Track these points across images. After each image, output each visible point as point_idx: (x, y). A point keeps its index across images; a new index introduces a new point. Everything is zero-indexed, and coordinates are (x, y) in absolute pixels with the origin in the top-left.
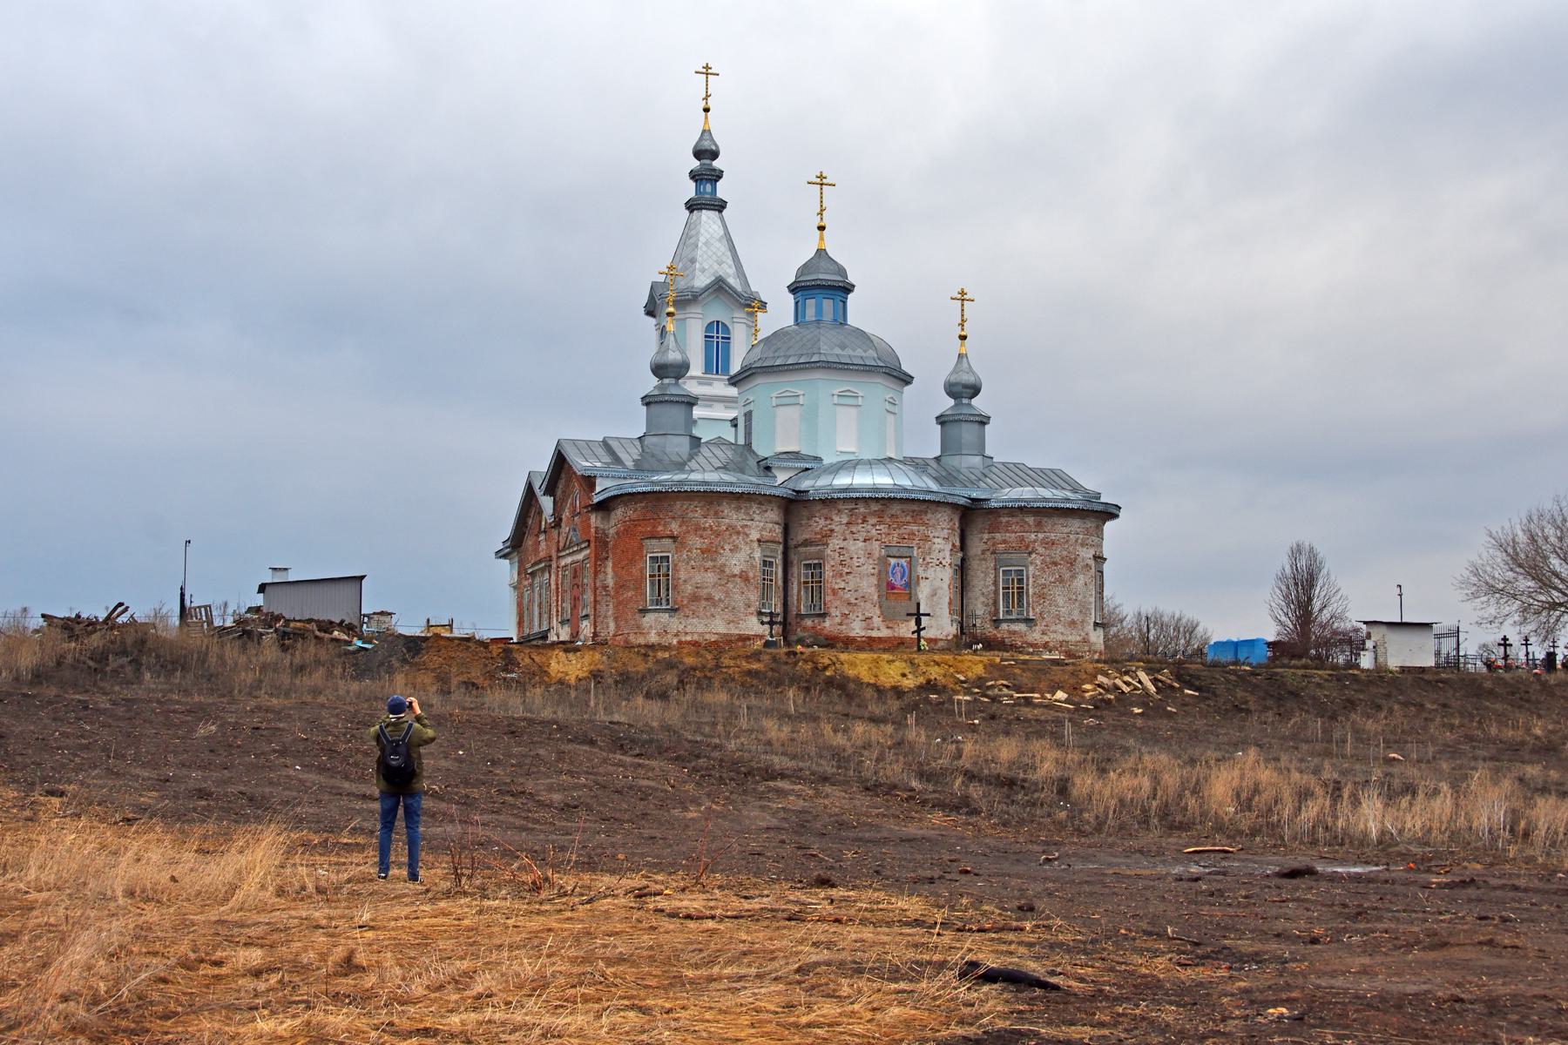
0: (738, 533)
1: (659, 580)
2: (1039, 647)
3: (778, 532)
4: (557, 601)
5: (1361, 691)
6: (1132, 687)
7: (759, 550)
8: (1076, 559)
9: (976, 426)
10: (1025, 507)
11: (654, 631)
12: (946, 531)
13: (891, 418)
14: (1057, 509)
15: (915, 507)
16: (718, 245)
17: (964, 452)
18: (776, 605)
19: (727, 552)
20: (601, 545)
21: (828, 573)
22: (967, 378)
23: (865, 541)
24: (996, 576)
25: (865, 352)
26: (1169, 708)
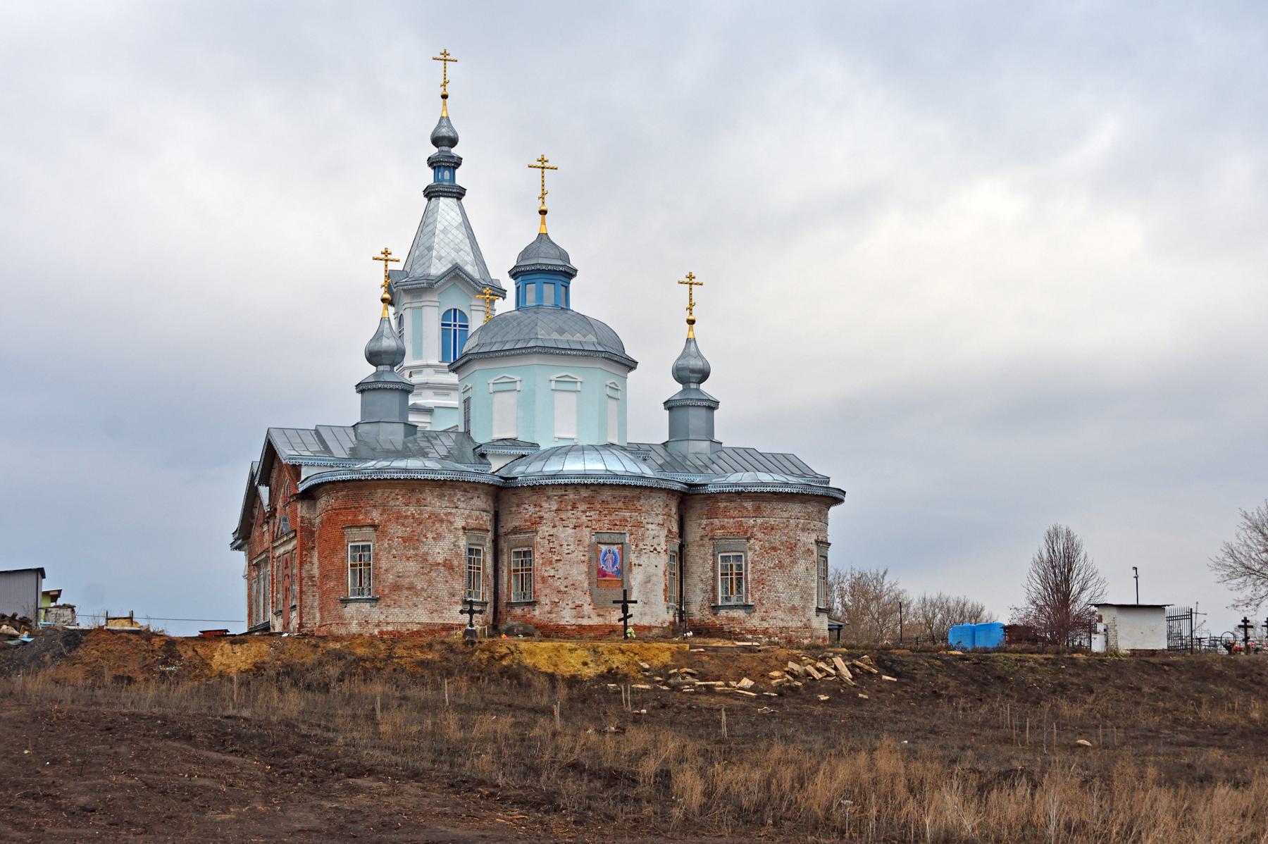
0: (442, 521)
1: (361, 570)
2: (758, 634)
3: (486, 520)
4: (273, 592)
5: (1078, 675)
6: (825, 674)
7: (465, 538)
8: (796, 544)
9: (703, 412)
10: (742, 492)
11: (355, 622)
12: (661, 517)
13: (612, 404)
14: (775, 493)
15: (627, 493)
16: (455, 232)
17: (691, 437)
18: (484, 594)
19: (430, 541)
20: (307, 534)
21: (537, 560)
22: (694, 363)
23: (575, 527)
24: (715, 563)
25: (585, 336)
26: (860, 695)
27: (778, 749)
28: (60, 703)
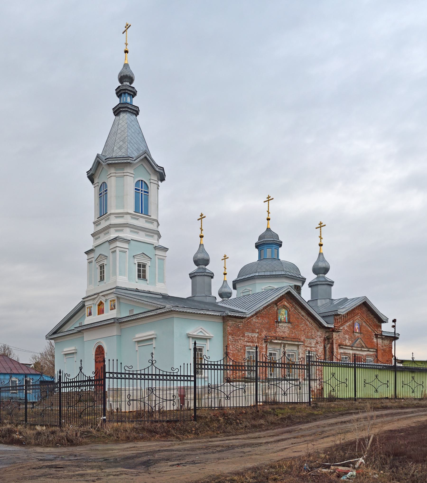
27: (260, 409)
28: (334, 441)
